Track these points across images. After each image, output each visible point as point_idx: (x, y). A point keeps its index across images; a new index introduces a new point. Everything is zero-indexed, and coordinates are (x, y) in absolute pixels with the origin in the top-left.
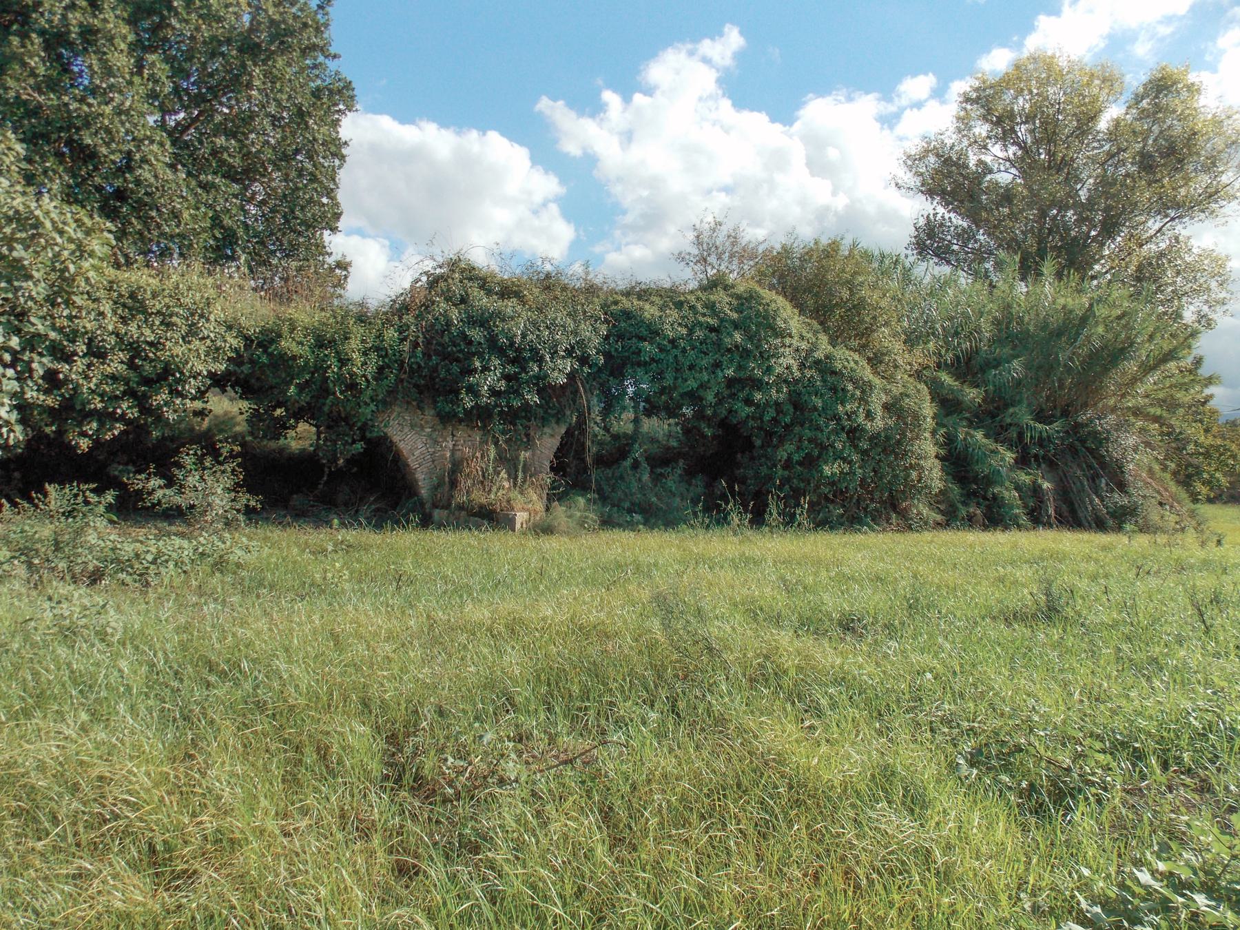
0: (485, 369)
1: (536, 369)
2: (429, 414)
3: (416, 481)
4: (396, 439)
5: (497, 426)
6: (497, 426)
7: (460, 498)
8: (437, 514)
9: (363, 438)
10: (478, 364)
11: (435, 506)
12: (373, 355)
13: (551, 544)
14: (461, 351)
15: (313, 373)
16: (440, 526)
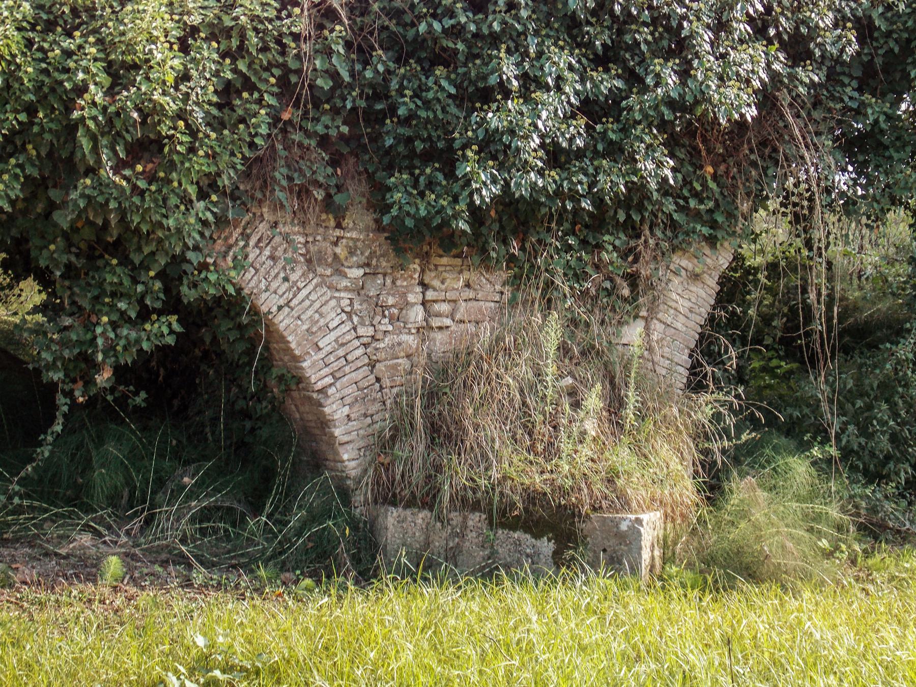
0: (530, 83)
1: (671, 80)
2: (358, 227)
3: (324, 423)
4: (267, 303)
5: (554, 261)
6: (554, 261)
7: (458, 474)
8: (399, 526)
9: (173, 304)
10: (509, 69)
11: (388, 496)
12: (208, 52)
13: (755, 615)
14: (456, 32)
15: (31, 110)
16: (425, 566)
